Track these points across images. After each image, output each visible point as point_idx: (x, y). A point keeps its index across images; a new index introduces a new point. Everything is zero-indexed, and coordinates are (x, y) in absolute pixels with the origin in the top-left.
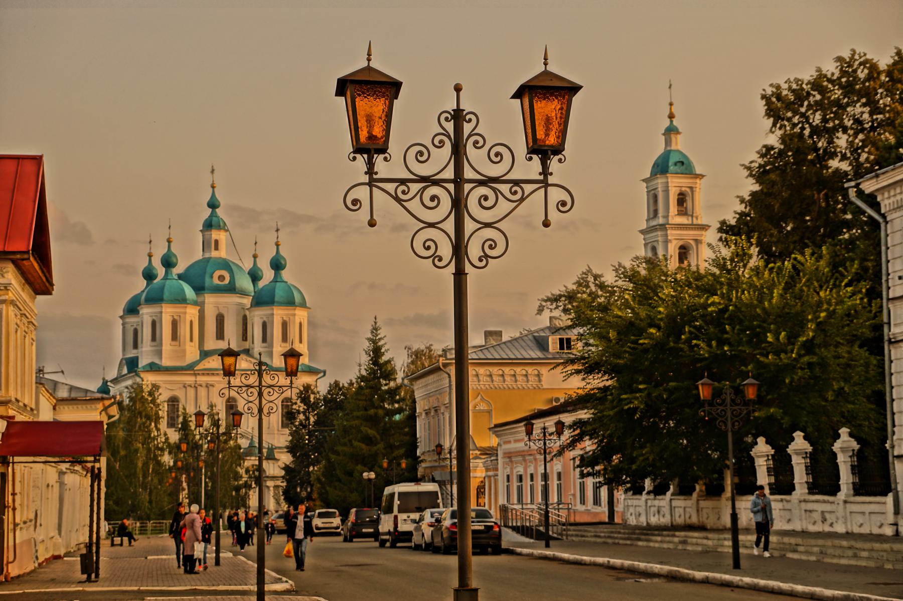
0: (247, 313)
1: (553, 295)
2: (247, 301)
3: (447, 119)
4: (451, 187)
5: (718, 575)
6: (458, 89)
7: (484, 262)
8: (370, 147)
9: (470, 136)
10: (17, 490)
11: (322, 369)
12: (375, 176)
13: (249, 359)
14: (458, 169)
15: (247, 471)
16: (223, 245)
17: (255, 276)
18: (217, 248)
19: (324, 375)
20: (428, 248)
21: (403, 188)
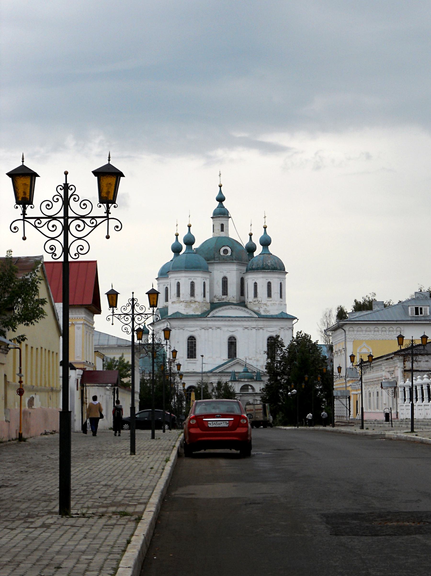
5: (51, 293)
6: (133, 293)
8: (24, 199)
10: (87, 397)
12: (26, 216)
13: (244, 309)
14: (66, 212)
17: (251, 249)
21: (39, 221)
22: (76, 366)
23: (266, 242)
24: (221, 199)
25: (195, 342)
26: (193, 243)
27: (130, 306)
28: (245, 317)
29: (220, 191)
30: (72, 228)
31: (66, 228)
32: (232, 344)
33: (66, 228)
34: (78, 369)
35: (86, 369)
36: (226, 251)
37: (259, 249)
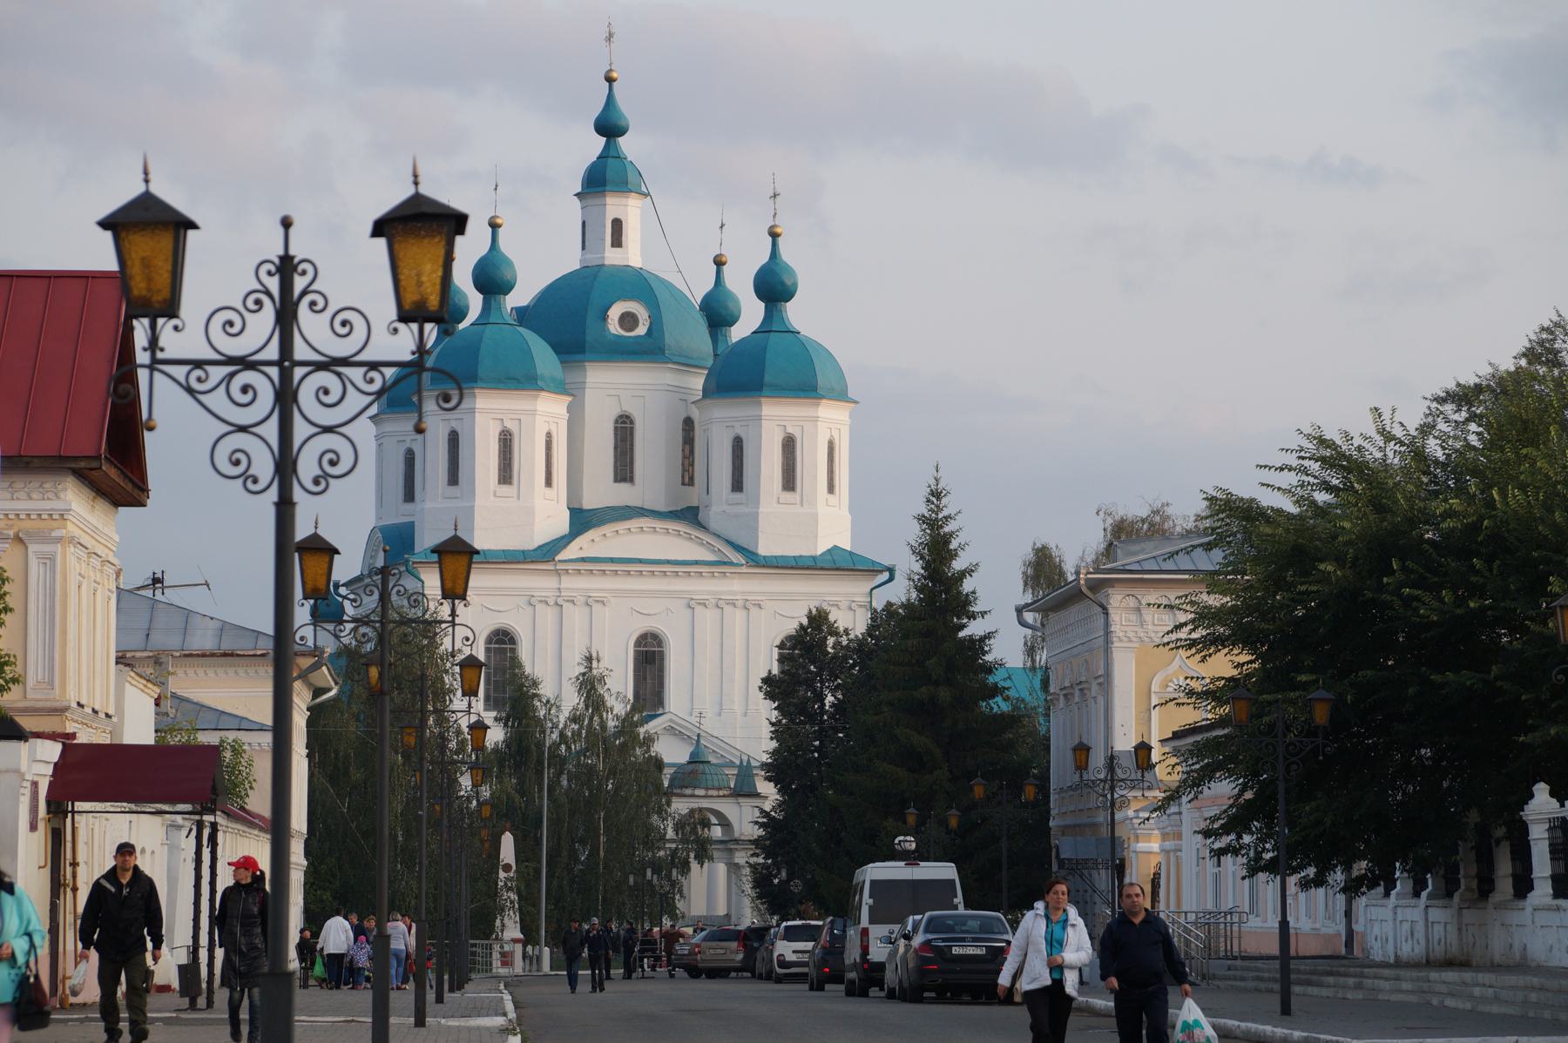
0: (695, 414)
1: (1459, 385)
2: (697, 382)
3: (270, 273)
4: (274, 372)
6: (286, 223)
7: (323, 484)
9: (304, 293)
10: (81, 858)
11: (887, 563)
13: (695, 533)
15: (679, 827)
16: (632, 233)
17: (717, 313)
18: (617, 242)
19: (891, 579)
20: (237, 463)
21: (198, 373)
22: (27, 723)
23: (774, 288)
24: (609, 127)
25: (513, 651)
26: (506, 288)
27: (269, 313)
28: (696, 563)
29: (610, 97)
30: (306, 396)
31: (286, 397)
32: (650, 657)
33: (286, 397)
34: (38, 735)
35: (73, 736)
36: (628, 320)
37: (750, 315)
